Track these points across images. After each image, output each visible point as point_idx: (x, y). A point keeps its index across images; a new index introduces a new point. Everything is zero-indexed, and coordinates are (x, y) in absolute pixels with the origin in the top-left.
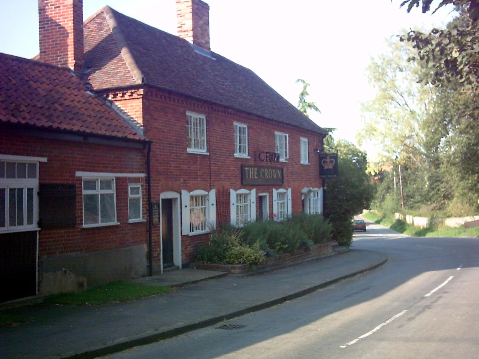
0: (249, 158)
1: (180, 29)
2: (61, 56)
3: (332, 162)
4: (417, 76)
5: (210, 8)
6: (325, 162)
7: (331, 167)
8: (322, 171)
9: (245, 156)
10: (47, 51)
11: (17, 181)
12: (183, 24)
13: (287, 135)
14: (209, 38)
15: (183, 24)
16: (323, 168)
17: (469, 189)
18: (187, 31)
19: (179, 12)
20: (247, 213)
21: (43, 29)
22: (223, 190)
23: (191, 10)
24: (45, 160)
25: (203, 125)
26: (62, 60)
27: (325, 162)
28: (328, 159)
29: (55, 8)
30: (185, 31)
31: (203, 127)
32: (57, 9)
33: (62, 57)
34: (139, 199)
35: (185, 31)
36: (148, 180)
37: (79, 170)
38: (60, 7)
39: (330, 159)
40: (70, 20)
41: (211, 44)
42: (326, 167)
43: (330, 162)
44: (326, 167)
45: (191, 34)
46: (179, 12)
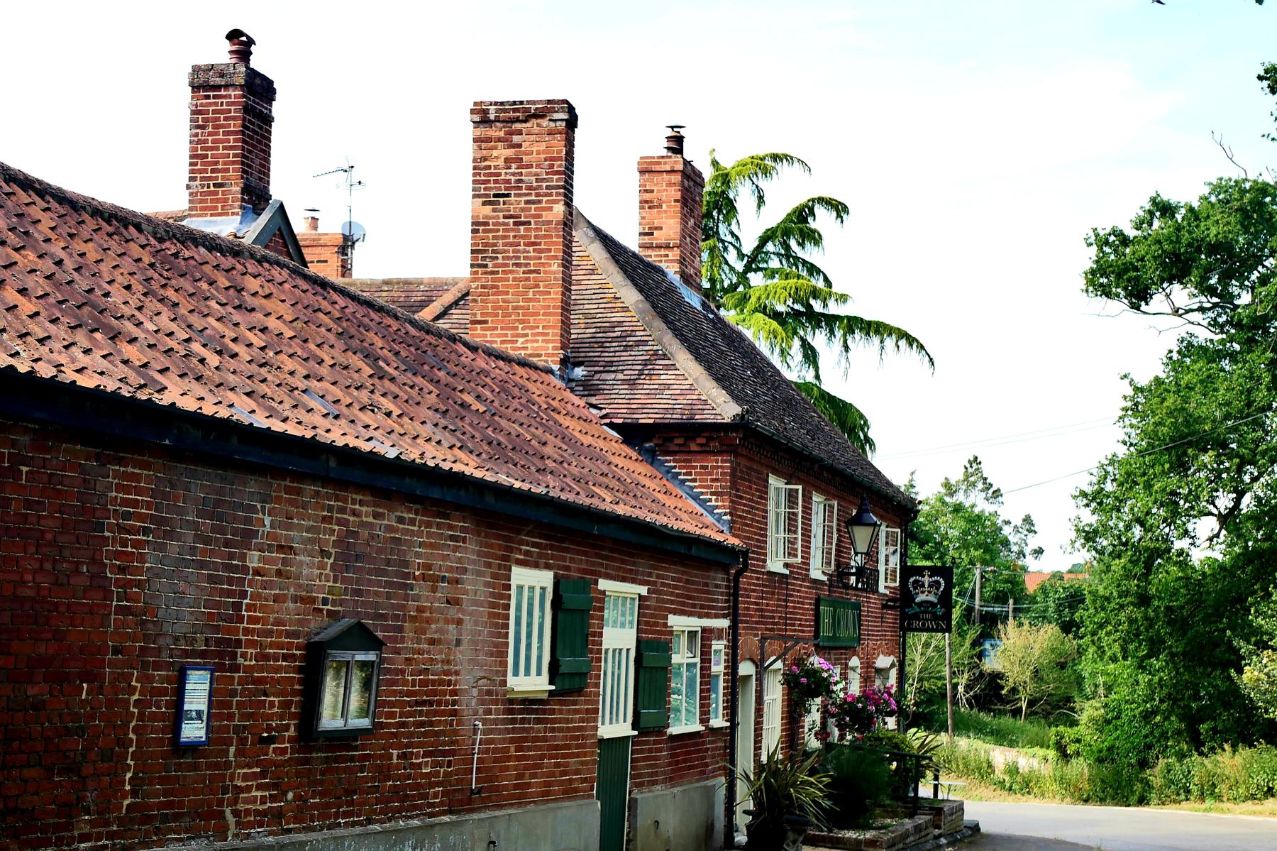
1: (647, 239)
2: (526, 335)
4: (734, 227)
10: (490, 319)
11: (1210, 809)
12: (656, 228)
13: (836, 503)
15: (656, 228)
18: (667, 247)
19: (647, 196)
21: (480, 270)
23: (678, 195)
24: (643, 590)
26: (529, 345)
28: (926, 578)
29: (515, 224)
30: (659, 247)
32: (522, 228)
33: (530, 338)
35: (659, 247)
36: (734, 627)
37: (675, 612)
38: (529, 223)
40: (555, 257)
45: (674, 254)
46: (647, 196)
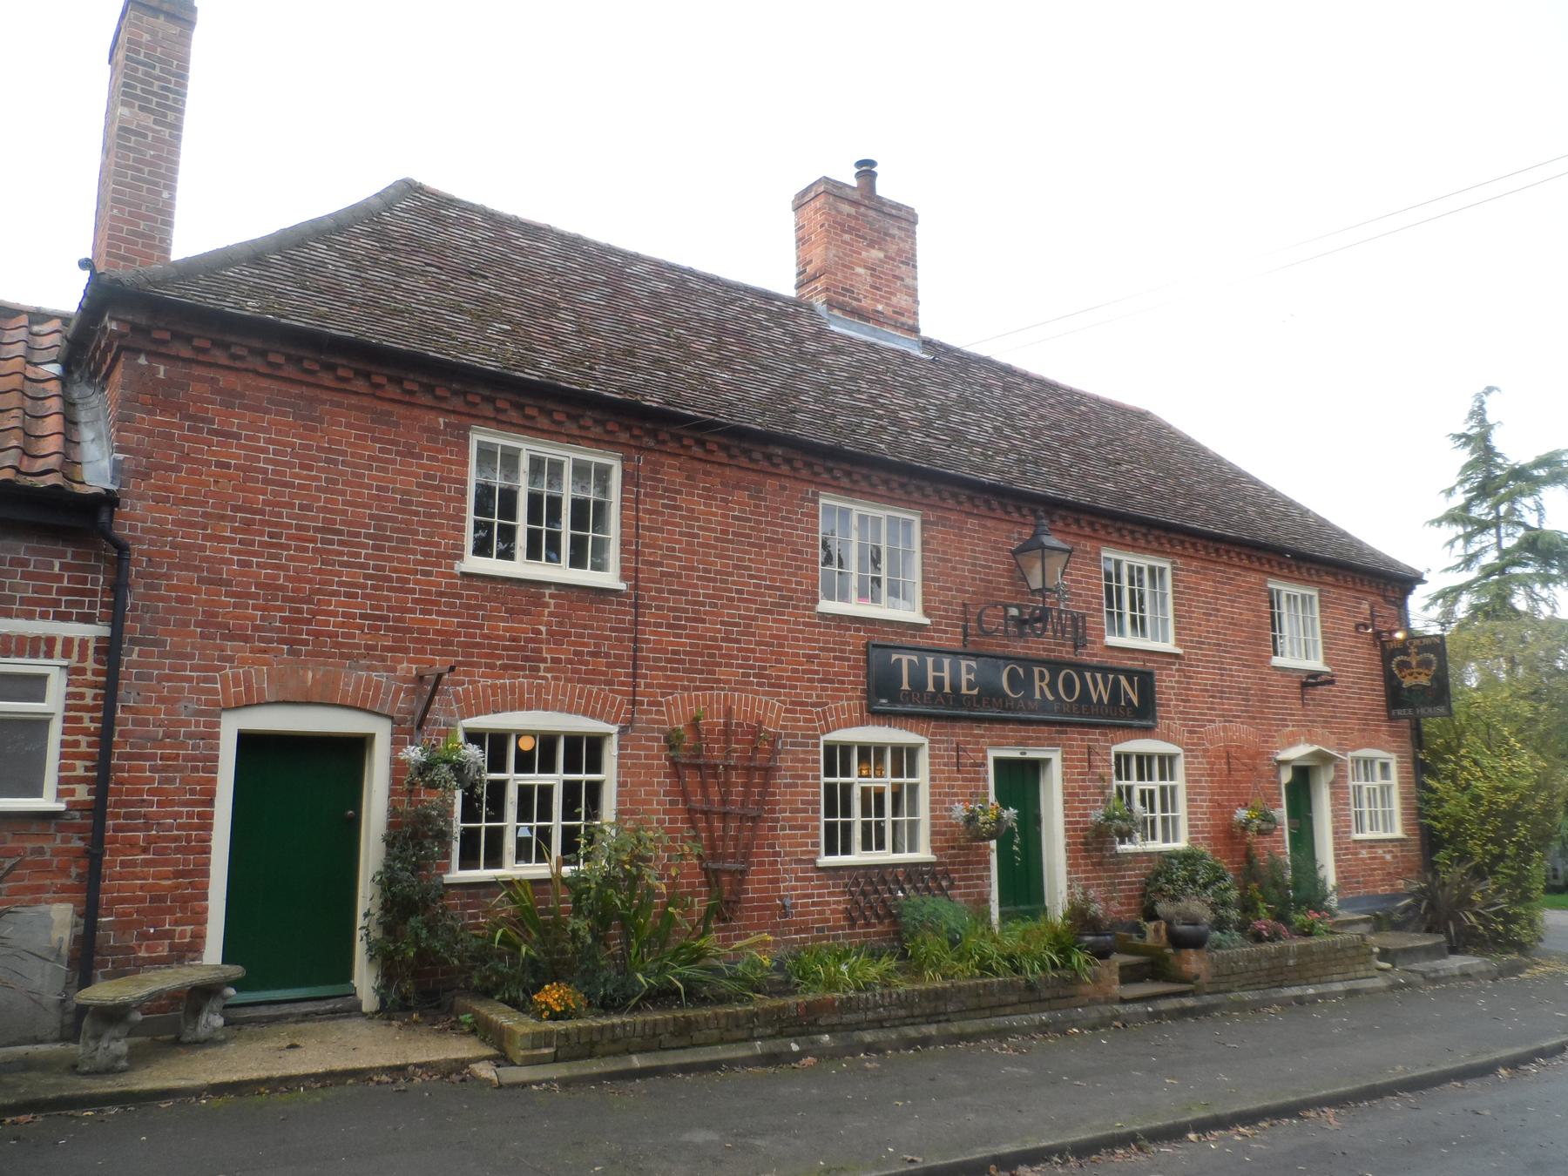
0: (927, 621)
3: (1425, 664)
5: (920, 219)
6: (1404, 665)
7: (1424, 681)
8: (1397, 698)
9: (911, 612)
14: (916, 302)
16: (1400, 683)
17: (697, 719)
20: (1174, 810)
22: (726, 724)
25: (1163, 605)
27: (1404, 665)
31: (1164, 613)
34: (39, 725)
36: (109, 651)
39: (1418, 654)
41: (921, 317)
42: (1408, 682)
43: (1420, 664)
44: (1408, 682)
